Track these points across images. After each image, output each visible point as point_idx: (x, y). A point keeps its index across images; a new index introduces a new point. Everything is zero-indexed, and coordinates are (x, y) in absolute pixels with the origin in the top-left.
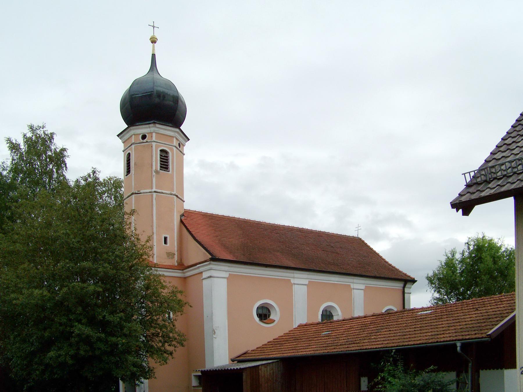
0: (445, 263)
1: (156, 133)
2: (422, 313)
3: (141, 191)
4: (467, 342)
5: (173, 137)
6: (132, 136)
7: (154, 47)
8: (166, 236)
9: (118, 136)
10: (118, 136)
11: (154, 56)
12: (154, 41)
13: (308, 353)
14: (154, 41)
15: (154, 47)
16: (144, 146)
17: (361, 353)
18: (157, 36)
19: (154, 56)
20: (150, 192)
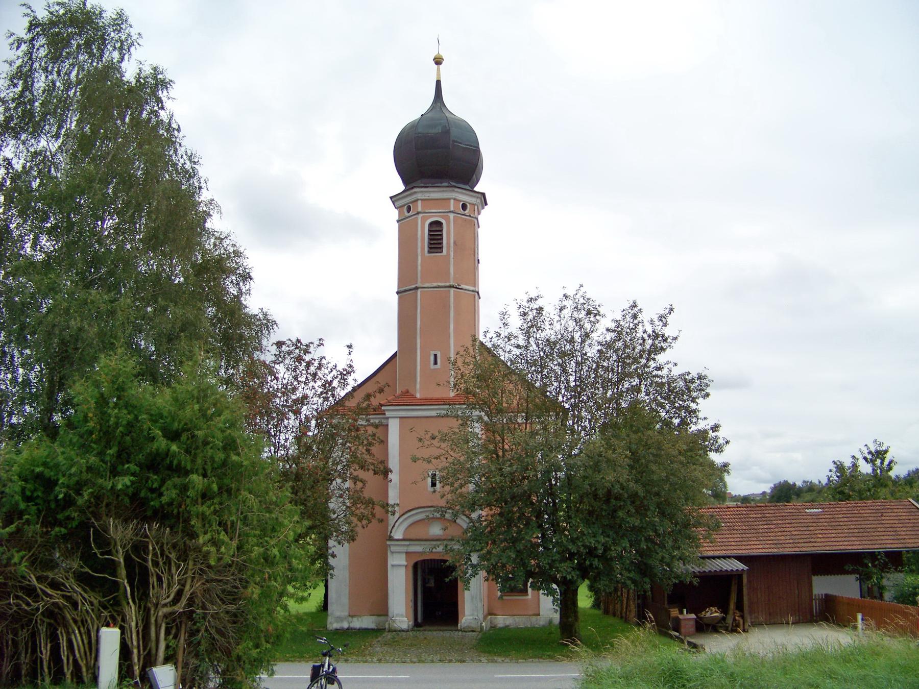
0: (157, 450)
1: (455, 199)
2: (812, 510)
3: (462, 286)
4: (526, 673)
5: (449, 199)
6: (418, 200)
7: (438, 70)
8: (435, 353)
9: (391, 198)
10: (391, 198)
11: (438, 83)
12: (438, 61)
13: (754, 551)
14: (438, 61)
15: (438, 70)
16: (465, 220)
17: (852, 553)
18: (443, 54)
19: (438, 83)
20: (473, 291)
